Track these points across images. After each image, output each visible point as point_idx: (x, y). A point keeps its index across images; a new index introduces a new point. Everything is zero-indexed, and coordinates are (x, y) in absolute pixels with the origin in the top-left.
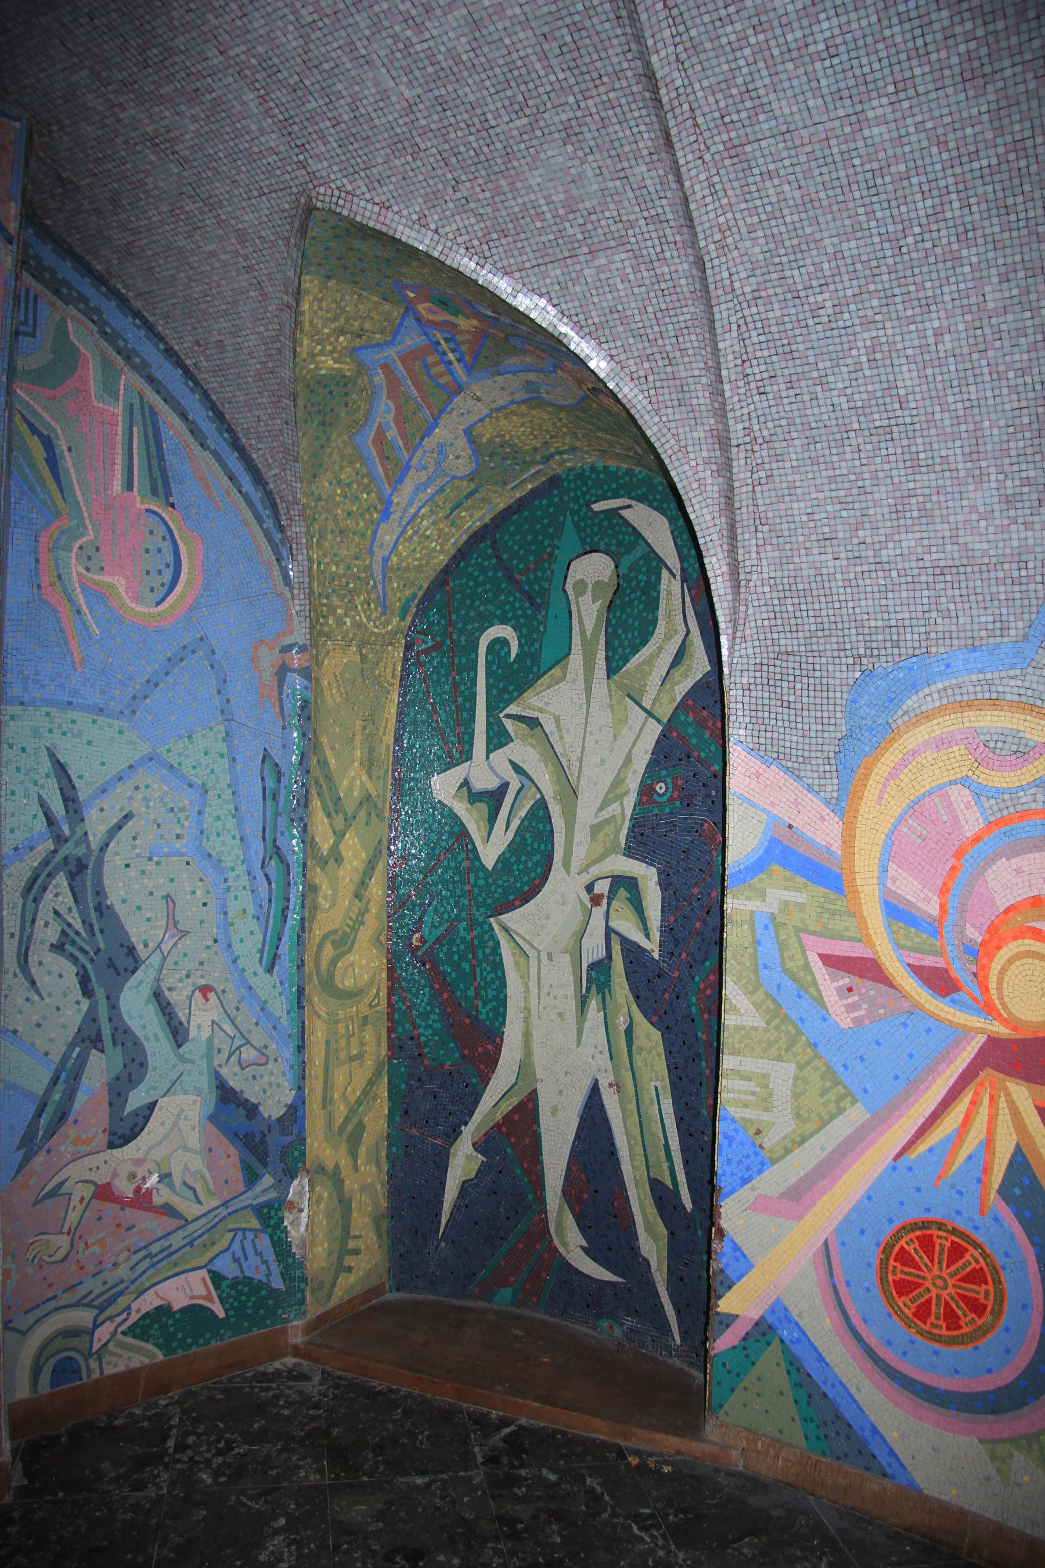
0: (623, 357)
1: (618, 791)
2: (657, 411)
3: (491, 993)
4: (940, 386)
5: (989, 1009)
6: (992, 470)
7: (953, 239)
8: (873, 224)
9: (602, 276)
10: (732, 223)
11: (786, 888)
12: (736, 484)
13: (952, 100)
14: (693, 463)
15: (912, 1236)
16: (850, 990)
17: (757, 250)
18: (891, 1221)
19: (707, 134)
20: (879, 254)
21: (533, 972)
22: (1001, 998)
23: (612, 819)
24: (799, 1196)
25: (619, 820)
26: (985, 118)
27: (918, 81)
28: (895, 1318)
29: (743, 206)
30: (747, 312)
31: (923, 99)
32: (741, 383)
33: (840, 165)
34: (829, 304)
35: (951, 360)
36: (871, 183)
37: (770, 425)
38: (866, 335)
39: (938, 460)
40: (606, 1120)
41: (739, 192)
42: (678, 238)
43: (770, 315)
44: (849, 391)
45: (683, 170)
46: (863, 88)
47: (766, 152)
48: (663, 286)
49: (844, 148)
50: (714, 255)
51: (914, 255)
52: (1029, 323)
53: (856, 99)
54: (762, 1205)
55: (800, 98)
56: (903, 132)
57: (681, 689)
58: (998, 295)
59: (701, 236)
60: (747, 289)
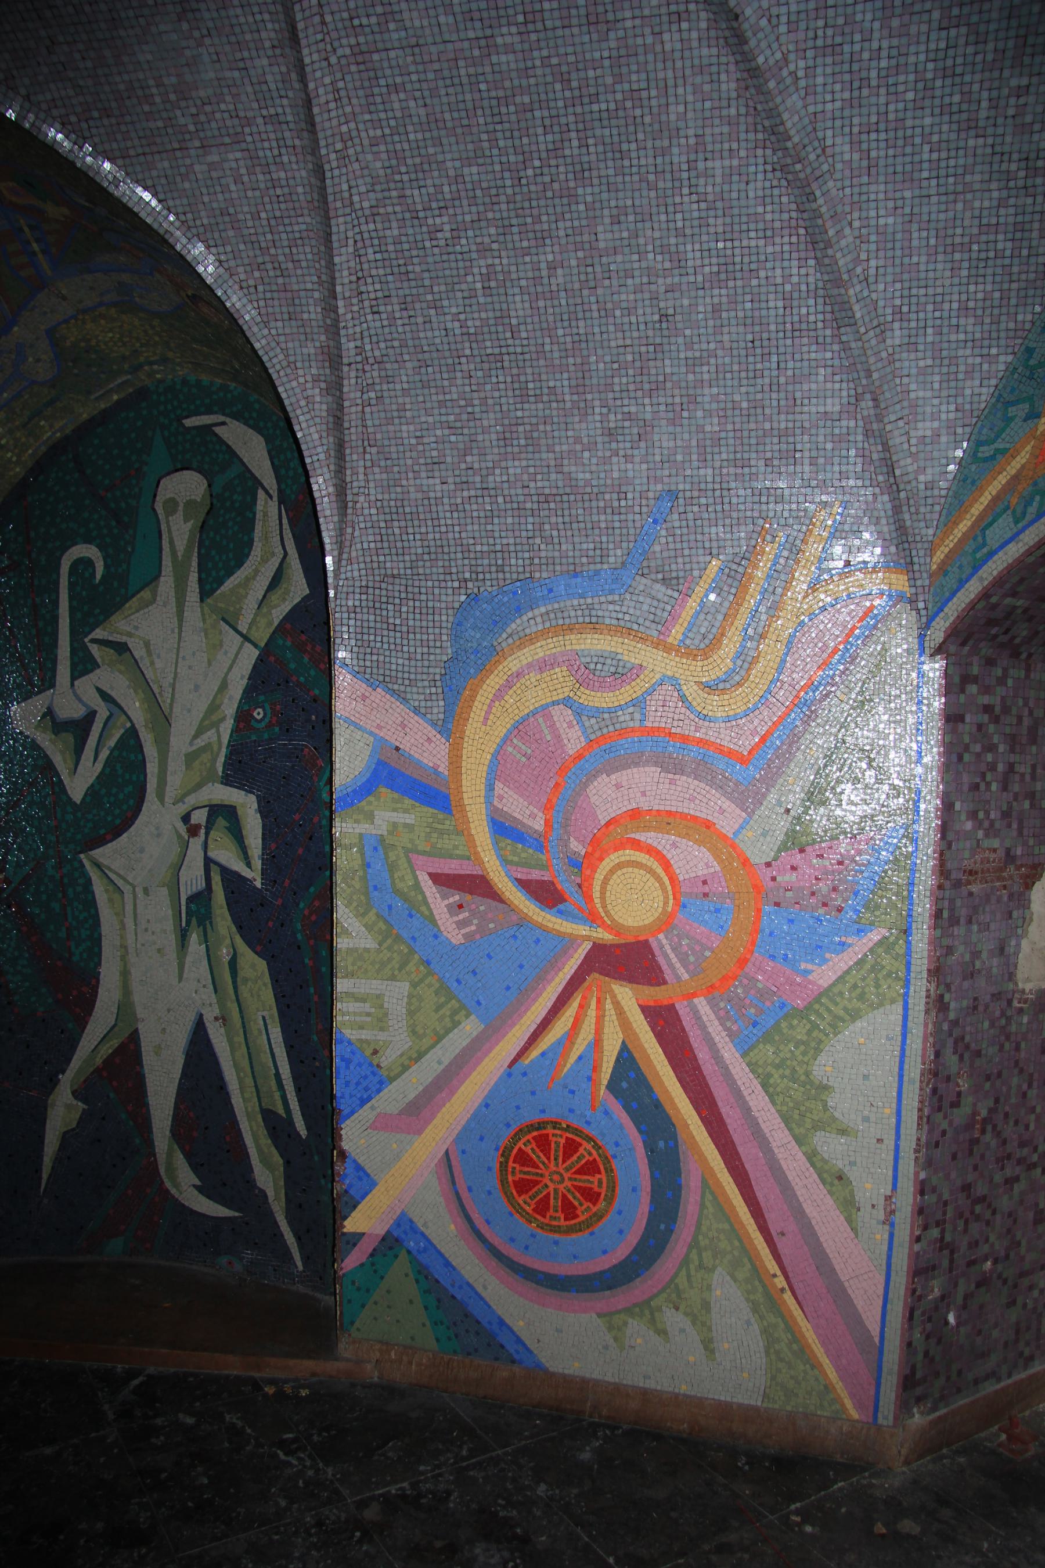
0: (232, 263)
1: (214, 718)
2: (266, 324)
3: (84, 934)
4: (551, 318)
5: (593, 918)
7: (571, 176)
8: (495, 152)
9: (214, 174)
10: (354, 134)
11: (394, 810)
12: (346, 404)
13: (577, 40)
14: (302, 380)
15: (529, 1137)
16: (460, 906)
17: (379, 164)
18: (508, 1125)
19: (334, 35)
20: (499, 183)
21: (129, 908)
22: (604, 907)
24: (418, 1113)
25: (215, 748)
26: (607, 63)
27: (547, 15)
28: (517, 1216)
29: (367, 117)
30: (364, 228)
31: (550, 34)
32: (355, 301)
33: (467, 88)
34: (447, 228)
35: (563, 294)
36: (496, 111)
37: (382, 345)
38: (482, 262)
40: (214, 1055)
41: (363, 101)
42: (297, 142)
43: (388, 233)
44: (462, 317)
45: (308, 69)
46: (493, 13)
47: (394, 63)
48: (279, 192)
49: (471, 71)
50: (334, 164)
51: (533, 188)
52: (636, 265)
53: (487, 23)
54: (383, 1123)
55: (432, 12)
56: (529, 64)
57: (280, 611)
58: (609, 236)
59: (322, 143)
60: (366, 204)
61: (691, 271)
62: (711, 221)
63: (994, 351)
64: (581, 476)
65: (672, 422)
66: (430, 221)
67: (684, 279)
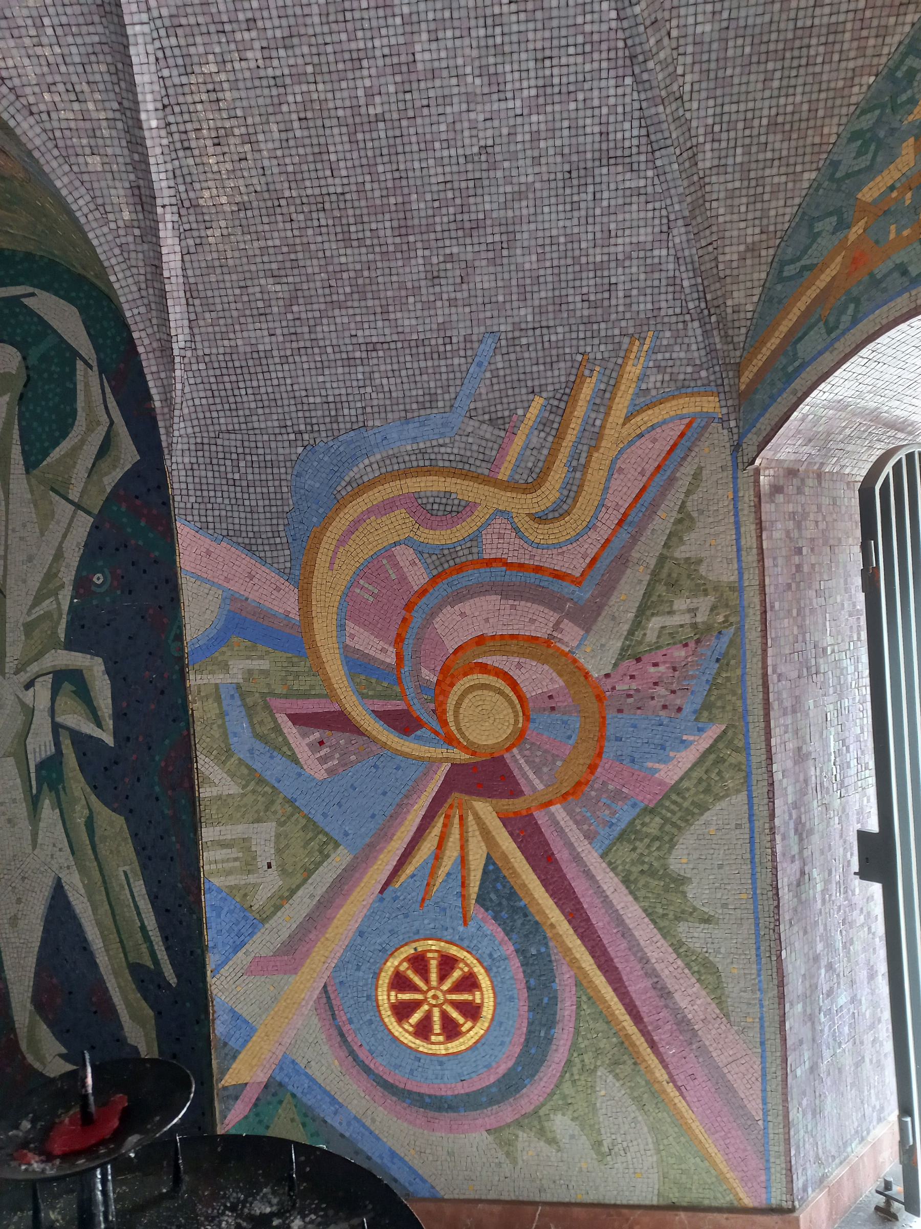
4: (370, 153)
5: (450, 740)
6: (419, 245)
14: (113, 226)
16: (321, 743)
23: (47, 616)
34: (257, 45)
38: (297, 89)
39: (368, 234)
52: (455, 90)
54: (260, 966)
61: (509, 95)
62: (531, 36)
63: (799, 168)
64: (407, 322)
65: (492, 262)
66: (238, 36)
67: (503, 105)
